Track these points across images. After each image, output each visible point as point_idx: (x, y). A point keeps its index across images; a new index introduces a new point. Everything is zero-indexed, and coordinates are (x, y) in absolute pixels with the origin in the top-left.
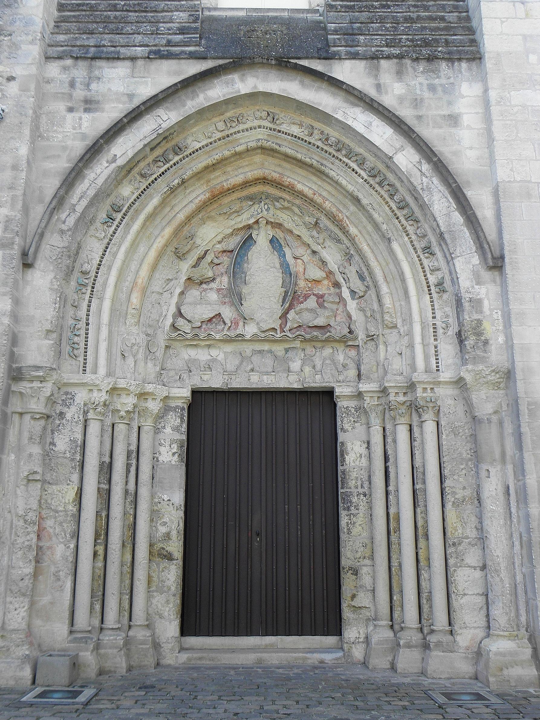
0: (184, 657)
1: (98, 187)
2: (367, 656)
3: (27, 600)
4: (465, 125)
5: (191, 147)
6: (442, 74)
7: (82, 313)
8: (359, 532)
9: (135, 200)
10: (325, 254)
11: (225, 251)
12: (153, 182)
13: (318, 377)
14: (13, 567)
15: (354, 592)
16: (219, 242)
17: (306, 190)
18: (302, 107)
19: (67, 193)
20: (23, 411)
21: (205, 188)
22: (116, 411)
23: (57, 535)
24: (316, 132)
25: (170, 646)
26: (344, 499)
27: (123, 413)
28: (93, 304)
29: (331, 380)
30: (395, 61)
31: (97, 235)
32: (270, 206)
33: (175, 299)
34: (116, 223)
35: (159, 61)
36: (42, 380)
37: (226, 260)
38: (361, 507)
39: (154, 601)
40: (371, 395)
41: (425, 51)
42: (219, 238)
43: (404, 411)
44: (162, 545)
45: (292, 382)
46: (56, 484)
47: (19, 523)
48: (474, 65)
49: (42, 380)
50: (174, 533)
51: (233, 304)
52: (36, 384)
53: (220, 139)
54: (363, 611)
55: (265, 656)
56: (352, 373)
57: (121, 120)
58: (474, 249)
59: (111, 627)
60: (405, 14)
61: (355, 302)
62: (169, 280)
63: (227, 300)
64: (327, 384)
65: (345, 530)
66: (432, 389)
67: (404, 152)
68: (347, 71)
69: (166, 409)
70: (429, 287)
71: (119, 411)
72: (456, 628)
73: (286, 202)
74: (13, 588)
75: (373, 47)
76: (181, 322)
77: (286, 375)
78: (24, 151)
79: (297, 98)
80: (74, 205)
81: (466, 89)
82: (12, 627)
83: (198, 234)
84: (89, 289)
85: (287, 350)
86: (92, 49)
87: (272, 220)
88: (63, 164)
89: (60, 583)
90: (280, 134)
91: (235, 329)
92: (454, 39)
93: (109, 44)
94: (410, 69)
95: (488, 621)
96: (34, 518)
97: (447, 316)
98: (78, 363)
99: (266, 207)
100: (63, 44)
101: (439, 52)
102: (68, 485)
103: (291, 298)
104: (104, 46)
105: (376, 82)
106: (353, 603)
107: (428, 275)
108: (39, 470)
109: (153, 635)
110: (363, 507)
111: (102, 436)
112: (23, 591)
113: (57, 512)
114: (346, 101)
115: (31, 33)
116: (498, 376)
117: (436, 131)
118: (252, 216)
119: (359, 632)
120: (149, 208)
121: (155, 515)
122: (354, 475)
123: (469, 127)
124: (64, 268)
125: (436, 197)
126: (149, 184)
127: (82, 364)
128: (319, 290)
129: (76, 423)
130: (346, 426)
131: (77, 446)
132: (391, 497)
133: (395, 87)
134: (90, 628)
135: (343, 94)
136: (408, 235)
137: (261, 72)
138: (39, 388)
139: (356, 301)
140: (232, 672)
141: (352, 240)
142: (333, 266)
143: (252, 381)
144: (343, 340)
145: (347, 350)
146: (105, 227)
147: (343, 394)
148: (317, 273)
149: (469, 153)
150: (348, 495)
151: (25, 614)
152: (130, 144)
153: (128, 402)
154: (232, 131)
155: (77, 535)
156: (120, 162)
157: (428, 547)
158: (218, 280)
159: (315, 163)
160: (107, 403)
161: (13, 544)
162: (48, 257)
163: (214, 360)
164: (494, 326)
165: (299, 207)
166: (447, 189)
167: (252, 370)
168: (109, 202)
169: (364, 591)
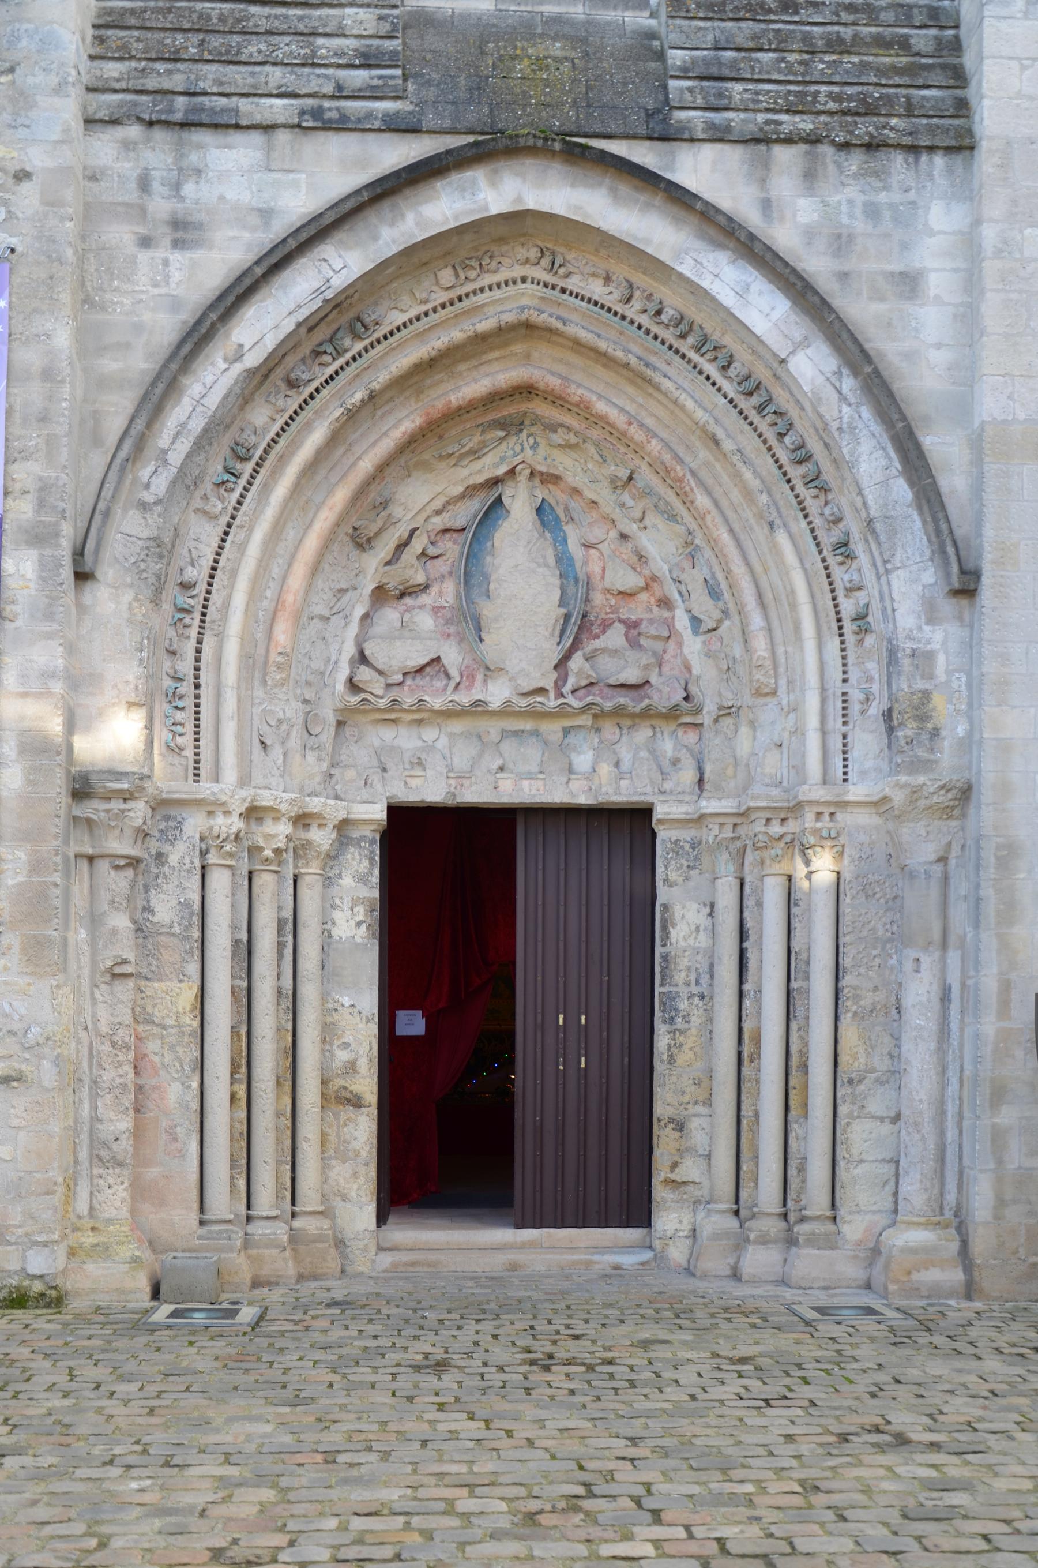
0: (386, 1260)
1: (210, 413)
2: (693, 1255)
5: (387, 321)
6: (894, 180)
7: (186, 667)
11: (446, 531)
15: (677, 1158)
16: (438, 512)
17: (613, 414)
20: (98, 851)
22: (254, 850)
24: (637, 294)
25: (361, 1244)
26: (665, 1004)
27: (268, 853)
29: (649, 789)
30: (803, 147)
32: (538, 439)
33: (353, 629)
34: (242, 482)
35: (321, 136)
36: (127, 797)
38: (693, 1019)
39: (333, 1174)
41: (864, 128)
42: (438, 504)
43: (780, 852)
44: (342, 1083)
45: (577, 793)
46: (160, 980)
48: (958, 159)
49: (127, 796)
51: (461, 639)
52: (116, 805)
53: (443, 306)
54: (690, 1188)
55: (520, 1257)
56: (688, 775)
57: (250, 269)
58: (928, 553)
59: (264, 1214)
60: (829, 28)
61: (699, 639)
62: (343, 591)
63: (452, 629)
64: (642, 798)
65: (665, 1057)
66: (832, 814)
67: (809, 351)
68: (698, 169)
70: (839, 620)
71: (260, 849)
72: (842, 1212)
73: (572, 434)
74: (104, 1153)
75: (760, 111)
76: (364, 674)
77: (565, 779)
79: (604, 226)
80: (165, 452)
82: (106, 1215)
83: (397, 496)
84: (197, 616)
85: (566, 731)
86: (181, 101)
87: (544, 469)
88: (140, 363)
89: (178, 1145)
90: (565, 296)
91: (469, 688)
92: (923, 98)
93: (215, 90)
94: (831, 168)
95: (896, 1203)
96: (127, 1039)
97: (870, 679)
98: (183, 761)
99: (531, 440)
100: (117, 86)
101: (892, 129)
102: (180, 981)
103: (578, 627)
104: (205, 94)
106: (673, 1176)
107: (841, 599)
108: (131, 956)
113: (164, 1027)
114: (702, 236)
115: (54, 66)
116: (950, 796)
118: (503, 459)
119: (681, 1222)
121: (328, 1032)
122: (684, 962)
124: (152, 579)
125: (866, 446)
126: (305, 401)
127: (191, 764)
129: (188, 872)
130: (673, 876)
131: (192, 914)
132: (747, 1002)
133: (800, 206)
134: (232, 1217)
135: (694, 220)
137: (530, 164)
138: (123, 811)
140: (470, 1284)
141: (700, 518)
142: (660, 566)
143: (501, 788)
144: (672, 714)
146: (222, 491)
147: (671, 817)
151: (124, 1194)
152: (269, 322)
154: (469, 287)
156: (253, 360)
157: (806, 1086)
158: (434, 590)
159: (633, 361)
160: (242, 834)
162: (121, 559)
163: (430, 748)
164: (951, 702)
165: (597, 445)
166: (887, 430)
167: (501, 769)
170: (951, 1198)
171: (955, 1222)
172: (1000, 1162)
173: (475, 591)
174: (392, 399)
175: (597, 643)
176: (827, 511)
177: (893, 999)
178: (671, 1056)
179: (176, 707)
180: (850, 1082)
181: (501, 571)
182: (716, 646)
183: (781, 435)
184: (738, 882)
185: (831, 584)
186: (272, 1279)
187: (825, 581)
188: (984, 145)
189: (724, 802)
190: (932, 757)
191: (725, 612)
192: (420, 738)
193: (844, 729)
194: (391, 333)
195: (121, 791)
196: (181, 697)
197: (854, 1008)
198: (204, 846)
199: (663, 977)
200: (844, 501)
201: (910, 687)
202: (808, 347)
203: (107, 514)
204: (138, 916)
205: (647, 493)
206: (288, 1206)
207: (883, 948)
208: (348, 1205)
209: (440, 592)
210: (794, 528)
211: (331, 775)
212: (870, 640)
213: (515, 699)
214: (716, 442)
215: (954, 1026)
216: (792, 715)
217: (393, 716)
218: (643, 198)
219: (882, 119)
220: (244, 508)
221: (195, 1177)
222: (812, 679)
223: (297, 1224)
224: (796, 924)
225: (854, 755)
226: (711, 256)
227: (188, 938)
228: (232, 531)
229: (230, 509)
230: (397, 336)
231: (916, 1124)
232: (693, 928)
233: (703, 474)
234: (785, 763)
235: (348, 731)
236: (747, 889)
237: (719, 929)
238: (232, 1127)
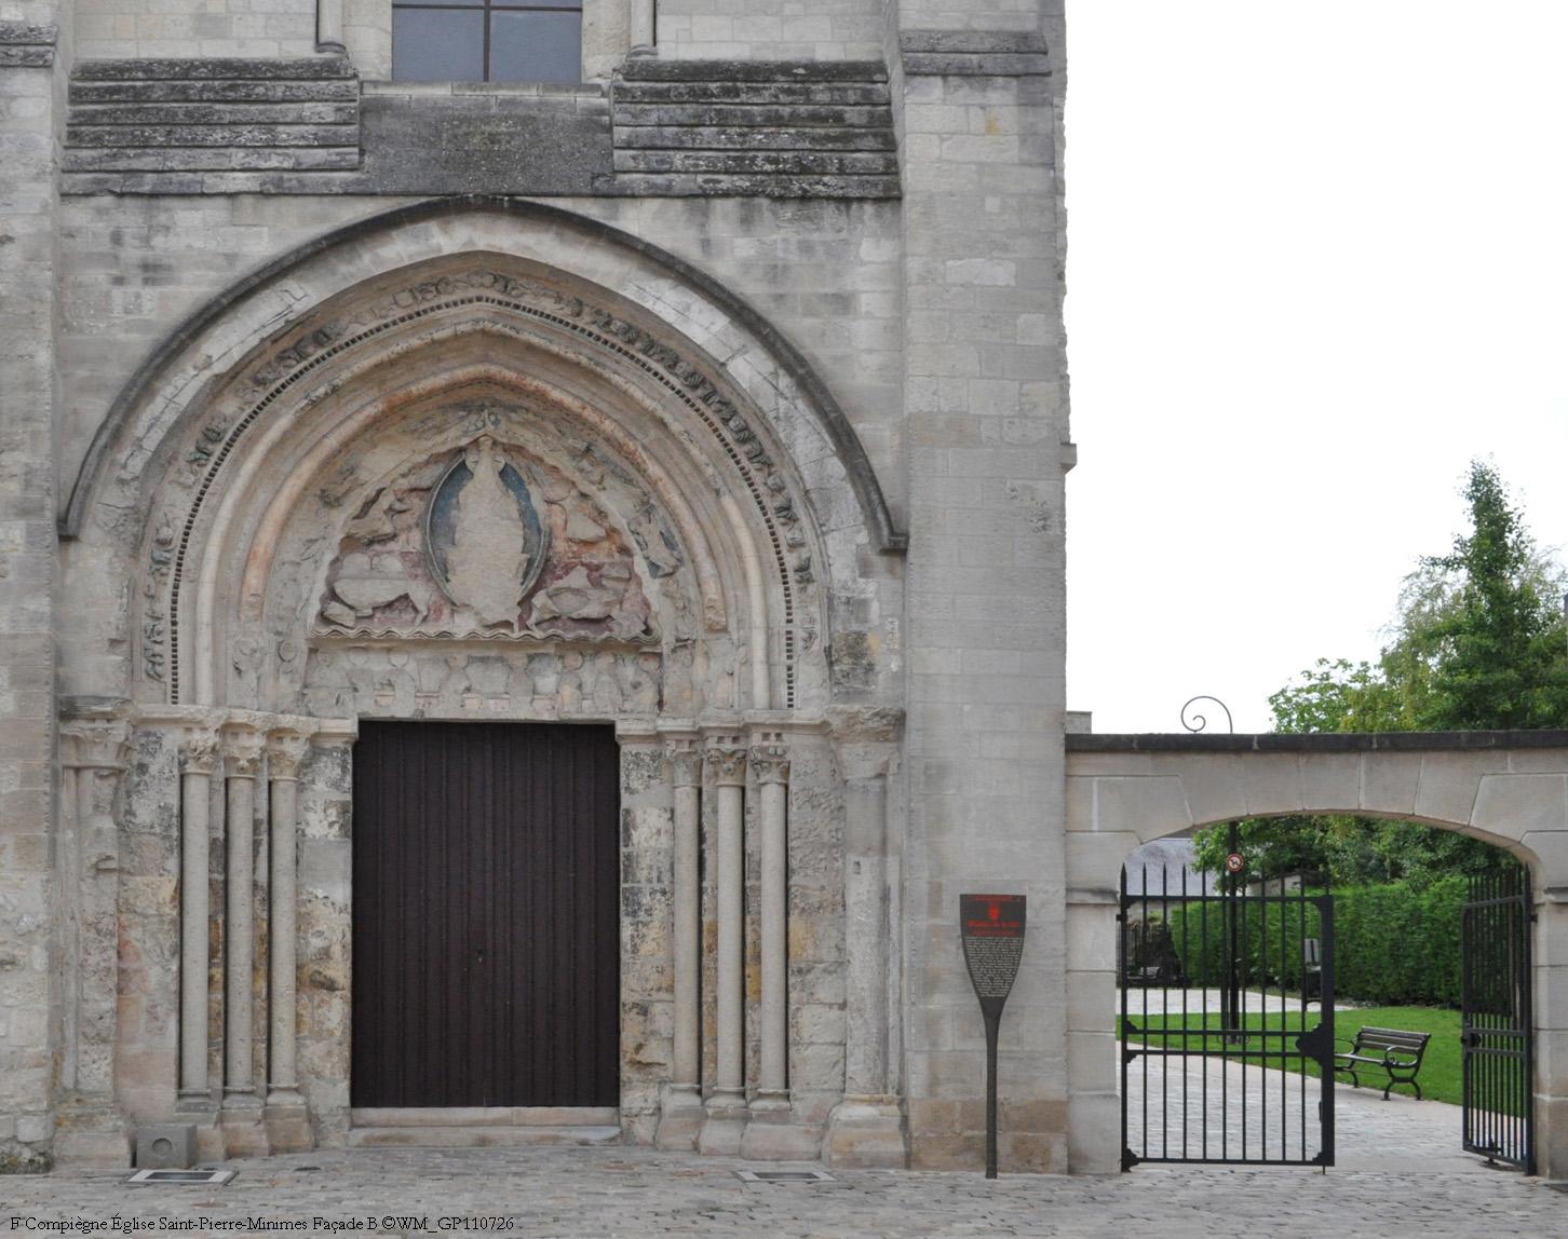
1: (182, 409)
3: (109, 1048)
4: (864, 309)
5: (348, 332)
6: (827, 223)
7: (164, 606)
8: (651, 949)
9: (246, 421)
10: (605, 500)
11: (413, 490)
12: (278, 391)
13: (586, 703)
14: (86, 1001)
16: (404, 476)
17: (568, 400)
18: (554, 279)
19: (125, 418)
21: (375, 393)
22: (230, 761)
23: (147, 952)
24: (587, 309)
26: (627, 899)
27: (243, 763)
28: (181, 591)
29: (609, 709)
30: (739, 199)
31: (182, 480)
32: (499, 417)
33: (324, 572)
34: (214, 459)
36: (109, 718)
37: (417, 504)
39: (307, 1052)
40: (678, 737)
42: (404, 469)
44: (316, 967)
46: (142, 874)
47: (88, 935)
48: (887, 208)
50: (337, 951)
51: (430, 579)
52: (100, 725)
53: (403, 320)
56: (648, 696)
58: (861, 518)
61: (658, 581)
63: (420, 571)
64: (603, 716)
65: (629, 947)
68: (636, 220)
70: (783, 570)
71: (238, 760)
72: (794, 1090)
76: (335, 609)
77: (529, 699)
80: (140, 440)
81: (867, 251)
84: (173, 567)
87: (505, 440)
88: (118, 373)
89: (159, 1024)
90: (517, 311)
91: (437, 619)
93: (182, 167)
94: (767, 214)
96: (111, 928)
97: (812, 621)
99: (493, 418)
101: (824, 185)
102: (161, 875)
103: (541, 570)
104: (172, 171)
105: (702, 237)
106: (638, 1058)
107: (785, 553)
110: (659, 913)
111: (210, 799)
112: (104, 1034)
113: (146, 916)
117: (808, 322)
118: (465, 433)
120: (273, 434)
121: (302, 921)
122: (645, 862)
123: (869, 315)
127: (170, 689)
128: (592, 556)
129: (167, 779)
130: (635, 784)
131: (171, 816)
133: (736, 247)
136: (751, 485)
138: (106, 730)
139: (661, 580)
141: (654, 483)
143: (467, 707)
146: (195, 466)
149: (866, 359)
150: (635, 892)
152: (234, 338)
154: (426, 305)
155: (180, 950)
156: (220, 367)
158: (402, 537)
159: (584, 361)
160: (218, 747)
161: (82, 966)
163: (400, 671)
166: (821, 419)
167: (468, 690)
168: (199, 426)
172: (934, 1044)
173: (441, 541)
174: (355, 390)
175: (560, 583)
176: (770, 481)
177: (838, 898)
178: (634, 946)
179: (155, 642)
180: (800, 971)
181: (466, 523)
182: (672, 588)
183: (725, 421)
184: (696, 791)
185: (775, 540)
186: (247, 1150)
187: (770, 538)
188: (907, 198)
189: (679, 721)
190: (867, 688)
191: (680, 560)
192: (389, 662)
193: (789, 662)
194: (353, 341)
195: (103, 713)
196: (159, 633)
197: (802, 905)
198: (182, 757)
199: (626, 873)
200: (784, 473)
201: (845, 629)
202: (746, 352)
203: (88, 490)
204: (121, 818)
205: (605, 461)
206: (263, 1083)
208: (323, 1083)
209: (408, 541)
211: (304, 695)
212: (811, 588)
213: (480, 631)
215: (894, 922)
216: (741, 649)
217: (363, 645)
218: (588, 240)
219: (816, 177)
220: (215, 479)
221: (174, 1053)
223: (272, 1099)
224: (749, 830)
225: (798, 685)
226: (653, 284)
227: (170, 837)
228: (205, 497)
229: (203, 481)
230: (359, 343)
231: (859, 1010)
232: (654, 831)
234: (736, 688)
235: (320, 657)
236: (705, 798)
237: (678, 832)
238: (210, 1008)
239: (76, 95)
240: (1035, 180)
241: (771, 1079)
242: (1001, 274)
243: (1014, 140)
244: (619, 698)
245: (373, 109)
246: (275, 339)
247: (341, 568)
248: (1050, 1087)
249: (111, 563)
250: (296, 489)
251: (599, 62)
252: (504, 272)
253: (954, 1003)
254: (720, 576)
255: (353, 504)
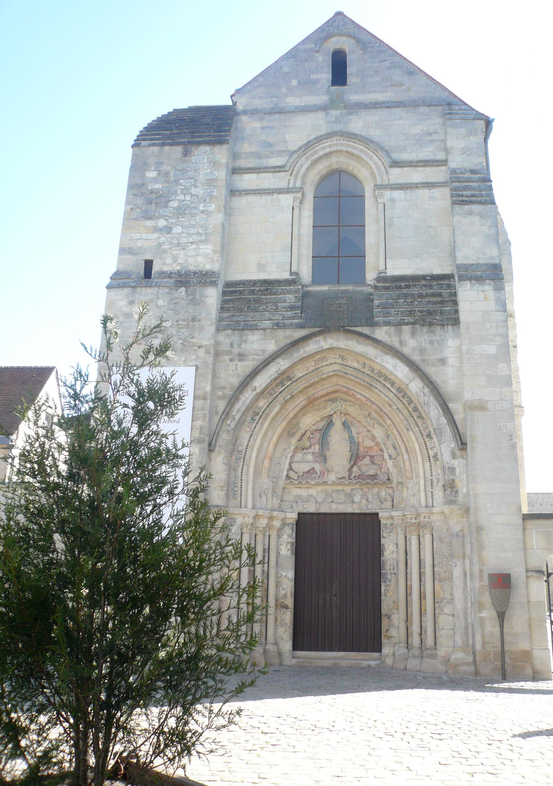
0: (294, 661)
8: (391, 594)
11: (316, 430)
13: (370, 506)
16: (313, 425)
24: (367, 366)
27: (261, 529)
30: (410, 326)
33: (288, 461)
34: (256, 422)
39: (279, 631)
42: (313, 423)
44: (282, 601)
50: (289, 595)
53: (312, 371)
54: (393, 639)
55: (338, 661)
56: (389, 504)
58: (452, 438)
61: (392, 461)
62: (285, 449)
63: (318, 459)
66: (429, 516)
68: (381, 333)
69: (284, 524)
70: (429, 457)
71: (259, 527)
72: (437, 646)
78: (208, 388)
80: (234, 416)
81: (451, 344)
84: (242, 460)
85: (352, 490)
94: (419, 331)
97: (439, 475)
103: (355, 458)
104: (248, 321)
107: (429, 451)
109: (278, 648)
118: (332, 410)
120: (274, 413)
121: (278, 585)
122: (389, 563)
130: (385, 535)
133: (412, 342)
135: (381, 347)
137: (335, 335)
142: (379, 440)
144: (384, 484)
145: (387, 489)
148: (371, 443)
153: (263, 522)
154: (319, 366)
156: (258, 390)
157: (425, 604)
158: (313, 447)
163: (311, 496)
167: (332, 502)
169: (394, 628)
170: (471, 642)
171: (472, 650)
172: (483, 629)
178: (385, 593)
182: (396, 464)
203: (218, 434)
207: (447, 558)
210: (414, 431)
212: (438, 463)
214: (391, 406)
222: (421, 475)
225: (435, 497)
233: (389, 414)
239: (224, 293)
240: (500, 316)
241: (430, 641)
242: (492, 349)
243: (494, 303)
244: (380, 504)
245: (305, 295)
246: (275, 380)
247: (20, 453)
248: (524, 645)
249: (223, 459)
250: (280, 432)
251: (370, 276)
252: (343, 354)
253: (488, 613)
254: (410, 459)
255: (297, 437)
